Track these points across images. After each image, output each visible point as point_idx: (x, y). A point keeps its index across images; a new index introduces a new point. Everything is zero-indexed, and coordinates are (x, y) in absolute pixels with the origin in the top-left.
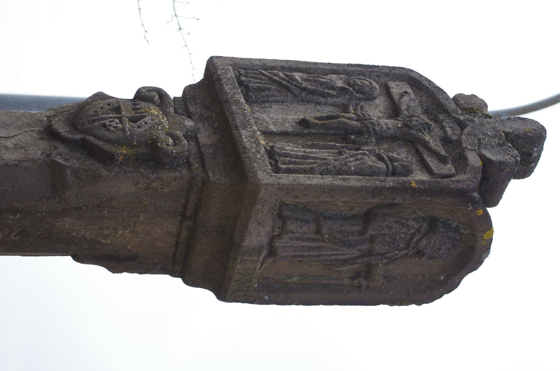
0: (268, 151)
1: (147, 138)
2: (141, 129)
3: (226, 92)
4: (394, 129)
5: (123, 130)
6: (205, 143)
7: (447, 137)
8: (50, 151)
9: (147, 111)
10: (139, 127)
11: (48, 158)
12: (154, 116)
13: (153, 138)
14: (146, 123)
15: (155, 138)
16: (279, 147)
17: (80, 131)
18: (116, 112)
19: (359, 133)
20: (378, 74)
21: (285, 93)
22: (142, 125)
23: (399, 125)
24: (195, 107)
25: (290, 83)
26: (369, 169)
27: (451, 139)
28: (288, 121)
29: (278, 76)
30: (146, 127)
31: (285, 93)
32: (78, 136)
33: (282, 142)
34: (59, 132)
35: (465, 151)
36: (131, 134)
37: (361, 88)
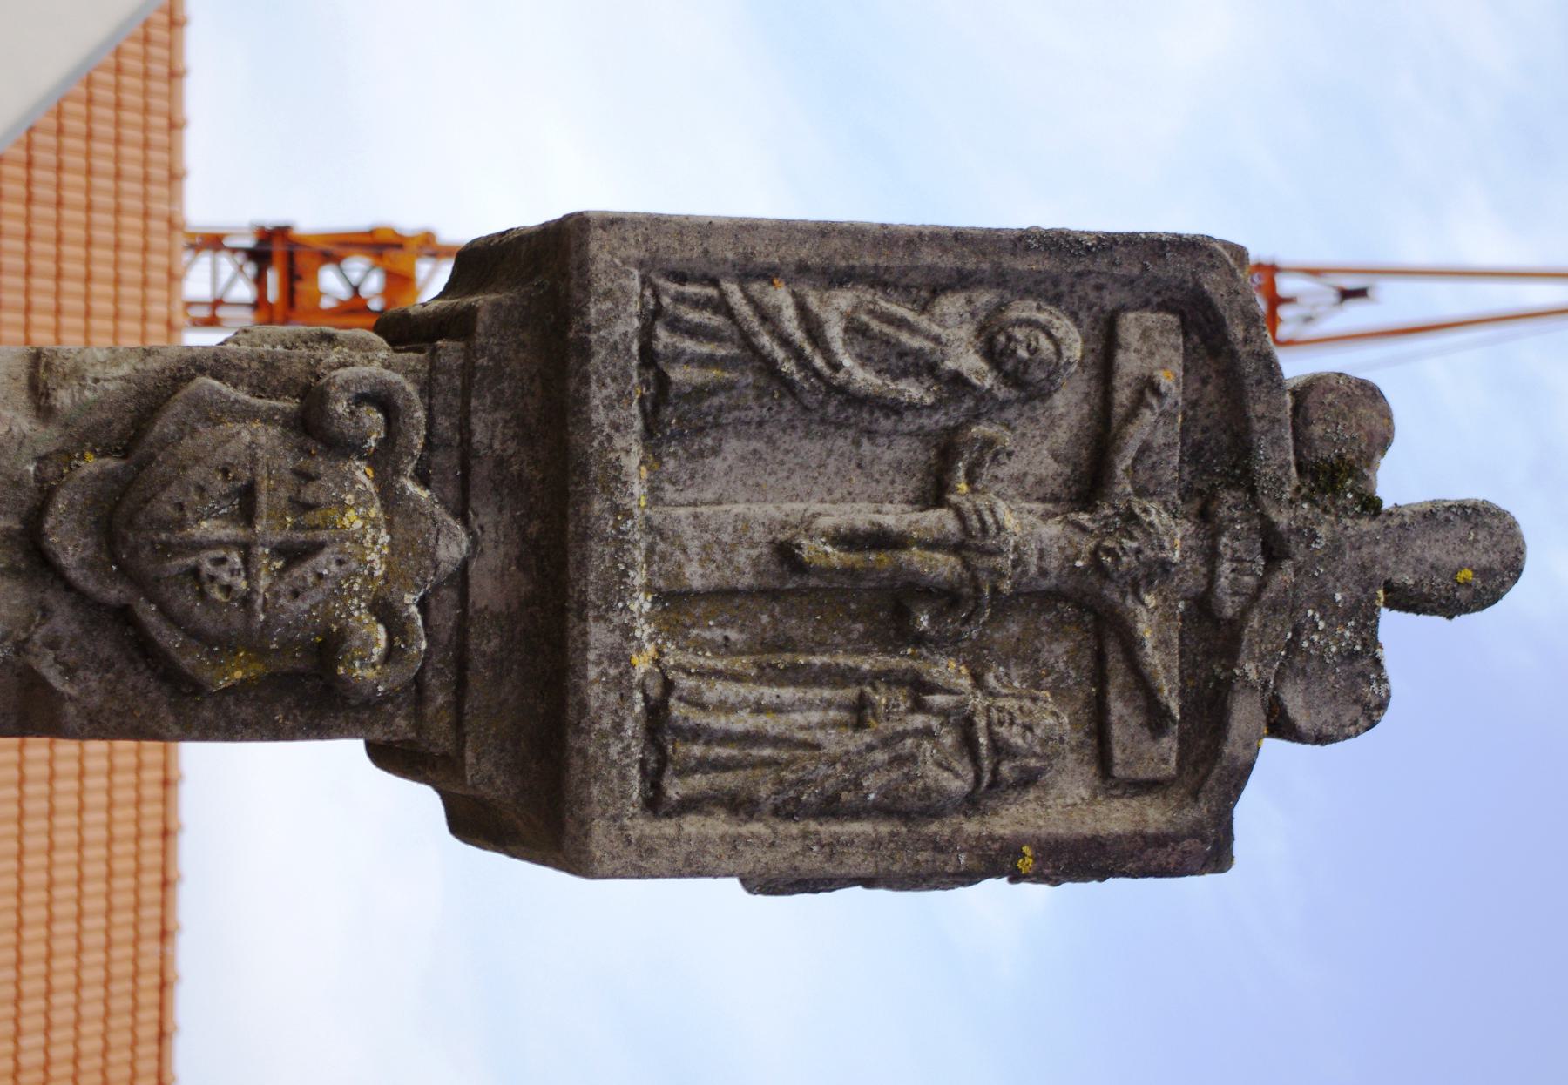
0: (652, 703)
1: (311, 631)
2: (299, 602)
3: (589, 420)
4: (1059, 576)
5: (247, 601)
6: (483, 605)
7: (1210, 601)
8: (26, 629)
9: (331, 523)
10: (296, 594)
11: (17, 653)
12: (348, 544)
13: (331, 630)
14: (320, 576)
15: (335, 628)
16: (685, 694)
17: (127, 573)
18: (241, 499)
19: (948, 598)
20: (1102, 280)
21: (776, 396)
22: (304, 588)
23: (1079, 563)
24: (490, 417)
25: (802, 362)
26: (920, 800)
27: (1217, 614)
28: (750, 538)
29: (774, 324)
30: (316, 596)
31: (776, 396)
32: (114, 593)
33: (710, 627)
34: (60, 565)
35: (1234, 692)
36: (266, 622)
37: (1021, 367)
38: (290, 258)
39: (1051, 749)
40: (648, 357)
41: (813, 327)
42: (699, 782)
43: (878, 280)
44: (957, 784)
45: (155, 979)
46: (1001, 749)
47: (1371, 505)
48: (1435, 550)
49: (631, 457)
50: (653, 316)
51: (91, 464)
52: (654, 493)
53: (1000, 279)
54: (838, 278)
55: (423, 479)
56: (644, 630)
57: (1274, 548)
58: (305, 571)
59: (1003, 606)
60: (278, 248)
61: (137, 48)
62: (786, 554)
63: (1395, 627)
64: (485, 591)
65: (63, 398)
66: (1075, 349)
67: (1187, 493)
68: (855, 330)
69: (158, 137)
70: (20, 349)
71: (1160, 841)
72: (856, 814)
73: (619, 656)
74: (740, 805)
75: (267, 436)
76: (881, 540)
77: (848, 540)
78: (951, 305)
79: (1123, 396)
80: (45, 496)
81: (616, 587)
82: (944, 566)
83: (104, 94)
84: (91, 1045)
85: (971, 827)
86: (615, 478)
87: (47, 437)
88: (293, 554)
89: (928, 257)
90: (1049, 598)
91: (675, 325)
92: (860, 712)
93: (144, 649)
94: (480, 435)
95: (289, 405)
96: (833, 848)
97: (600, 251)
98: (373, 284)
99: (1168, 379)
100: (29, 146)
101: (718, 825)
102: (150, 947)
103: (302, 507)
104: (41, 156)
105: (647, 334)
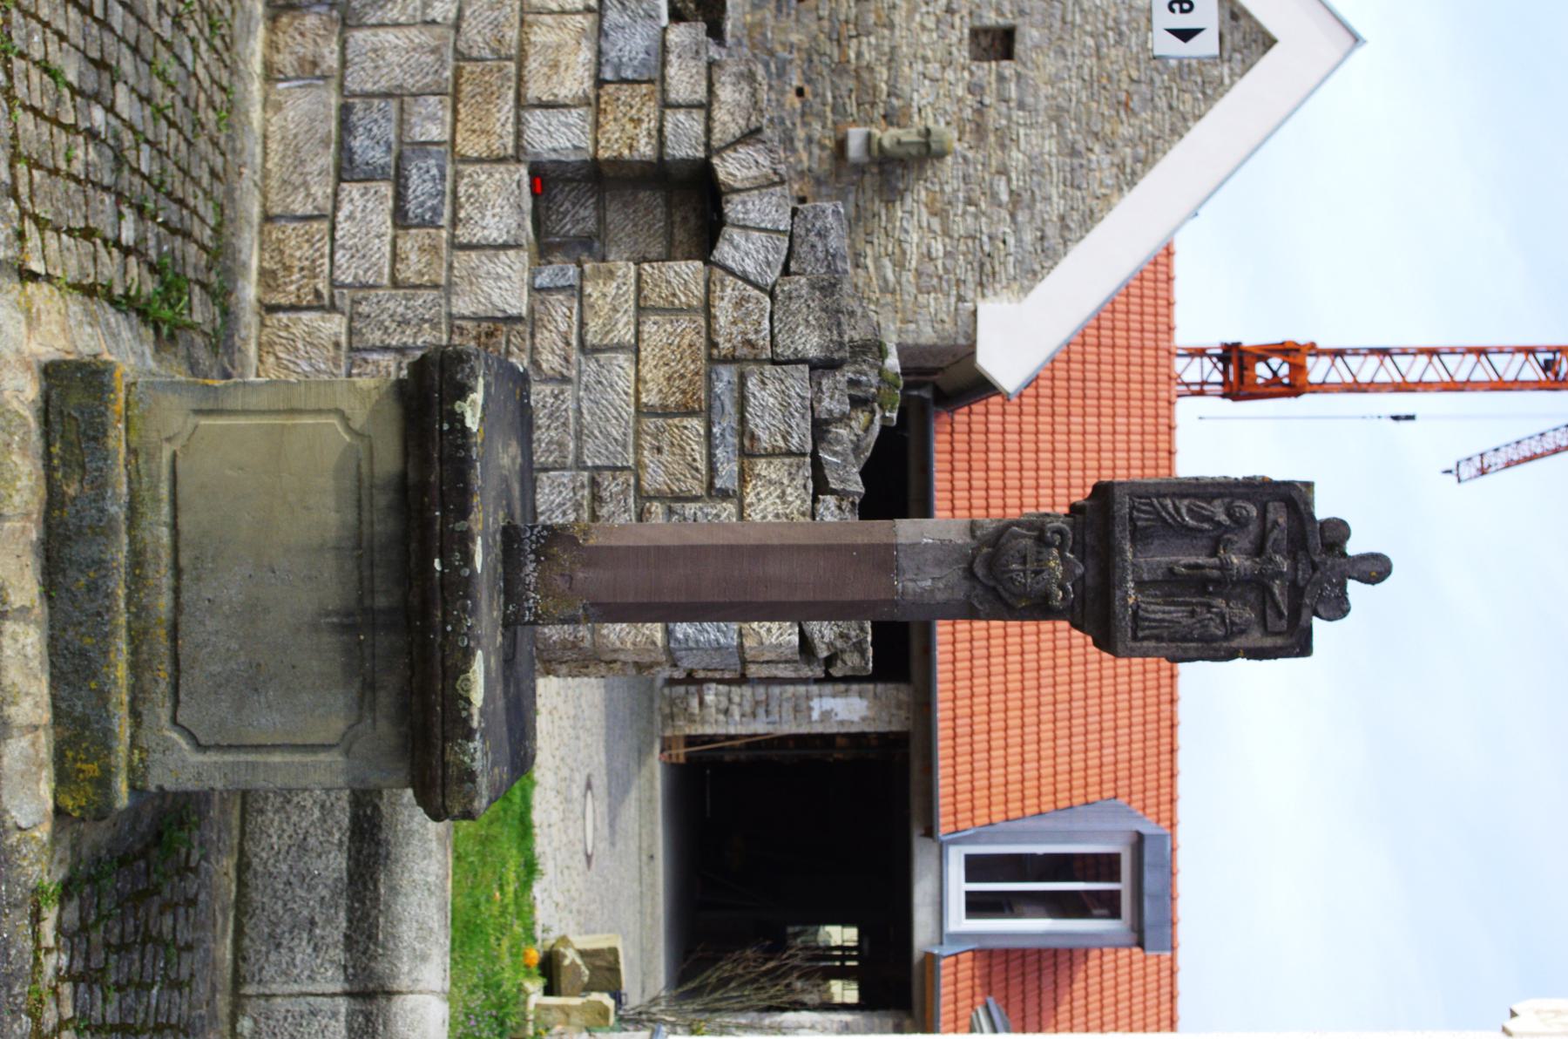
17: (995, 578)
19: (1218, 582)
32: (992, 583)
38: (1241, 360)
39: (1248, 622)
40: (1131, 519)
41: (1177, 510)
42: (1147, 632)
43: (1196, 496)
44: (1220, 633)
45: (1168, 723)
46: (1233, 623)
47: (1344, 555)
48: (1364, 567)
49: (1128, 546)
50: (1132, 508)
51: (985, 550)
52: (1134, 556)
53: (1231, 495)
54: (1183, 496)
55: (1072, 552)
56: (1131, 592)
57: (1314, 567)
58: (1039, 577)
59: (1235, 584)
60: (1234, 355)
61: (1137, 283)
62: (1171, 570)
63: (1353, 587)
64: (1089, 581)
65: (978, 533)
66: (1254, 512)
67: (1289, 552)
68: (1190, 510)
69: (1162, 310)
70: (967, 521)
71: (1281, 648)
72: (1192, 640)
73: (1124, 599)
74: (1159, 639)
75: (1029, 542)
76: (1197, 566)
77: (1187, 566)
78: (1217, 502)
79: (1269, 525)
80: (974, 557)
81: (1124, 580)
82: (1216, 573)
83: (1091, 340)
84: (1137, 754)
85: (1225, 644)
86: (1123, 552)
87: (974, 543)
88: (1037, 573)
89: (1210, 489)
90: (1248, 582)
91: (1139, 510)
92: (1193, 614)
93: (1000, 598)
94: (1087, 539)
95: (1035, 534)
96: (1185, 650)
97: (1117, 491)
98: (1284, 370)
99: (1281, 521)
100: (1068, 352)
101: (1152, 644)
102: (1165, 707)
103: (1038, 561)
104: (1089, 340)
105: (1131, 513)
